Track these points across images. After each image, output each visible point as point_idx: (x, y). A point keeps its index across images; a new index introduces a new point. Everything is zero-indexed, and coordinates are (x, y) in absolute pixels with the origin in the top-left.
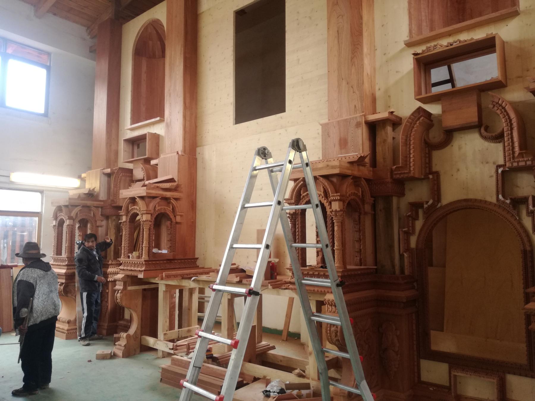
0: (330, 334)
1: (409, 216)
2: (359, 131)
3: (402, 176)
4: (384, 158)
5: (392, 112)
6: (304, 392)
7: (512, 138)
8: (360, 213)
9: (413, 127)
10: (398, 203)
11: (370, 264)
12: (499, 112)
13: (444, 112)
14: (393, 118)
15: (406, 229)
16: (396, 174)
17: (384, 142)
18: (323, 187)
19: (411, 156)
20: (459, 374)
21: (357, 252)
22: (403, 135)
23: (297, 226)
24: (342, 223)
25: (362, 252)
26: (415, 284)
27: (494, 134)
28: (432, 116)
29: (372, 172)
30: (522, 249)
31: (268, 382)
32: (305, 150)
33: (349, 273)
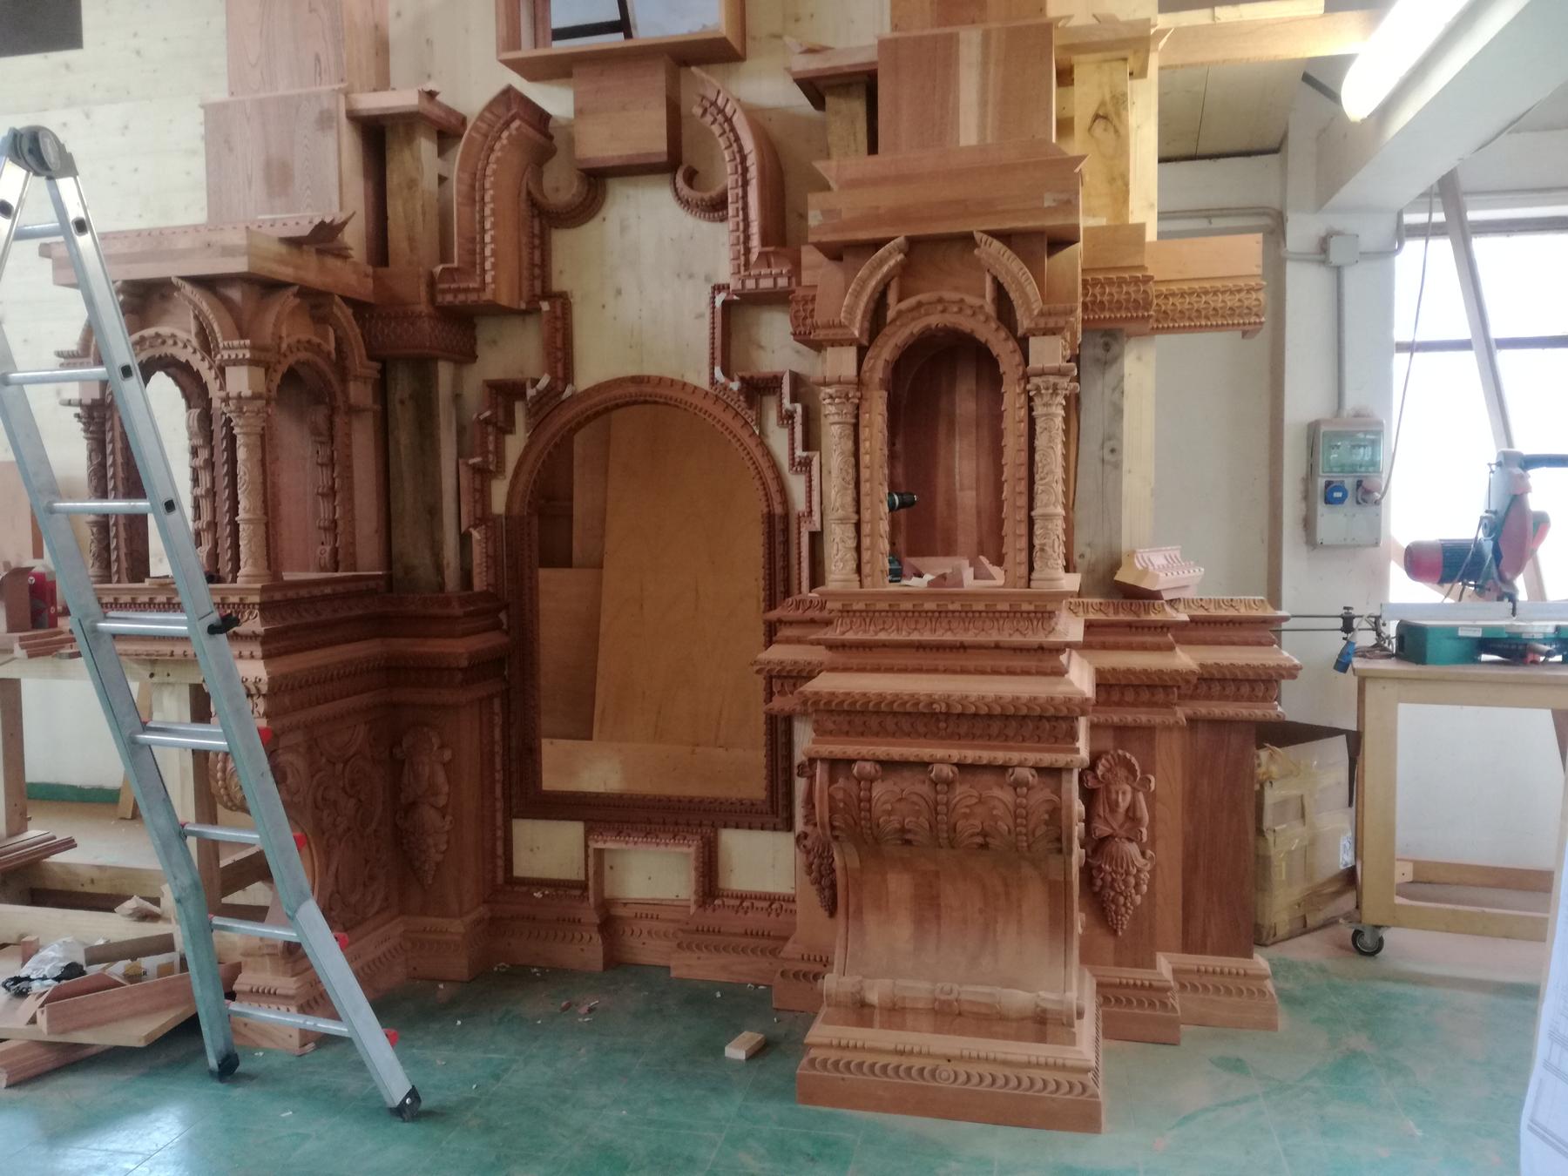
0: (224, 780)
1: (487, 421)
2: (330, 142)
3: (461, 297)
4: (411, 240)
5: (431, 95)
6: (149, 963)
7: (745, 208)
8: (333, 410)
9: (492, 149)
10: (457, 382)
11: (369, 563)
12: (716, 129)
13: (579, 112)
14: (435, 112)
15: (477, 460)
16: (444, 292)
17: (410, 188)
18: (196, 317)
19: (488, 238)
20: (609, 845)
21: (325, 529)
22: (461, 169)
23: (109, 448)
24: (262, 436)
25: (340, 529)
26: (503, 616)
27: (706, 196)
28: (551, 124)
29: (370, 281)
30: (766, 510)
31: (28, 950)
32: (69, 167)
33: (291, 594)
